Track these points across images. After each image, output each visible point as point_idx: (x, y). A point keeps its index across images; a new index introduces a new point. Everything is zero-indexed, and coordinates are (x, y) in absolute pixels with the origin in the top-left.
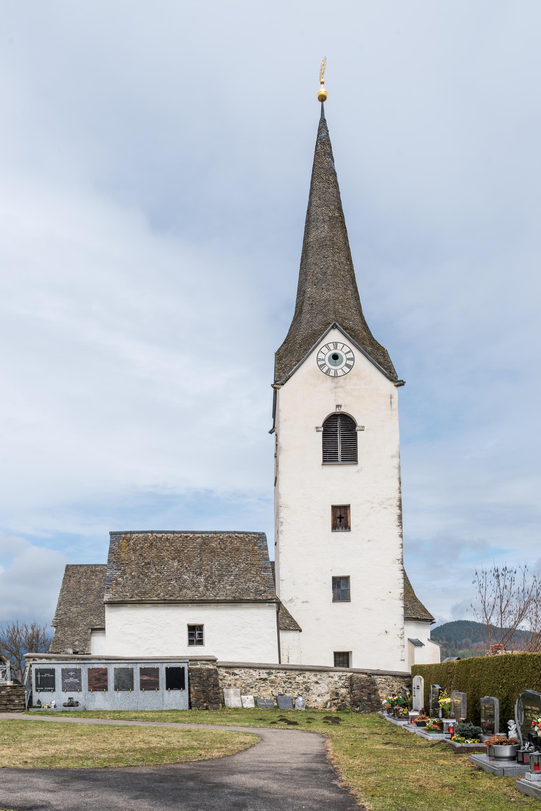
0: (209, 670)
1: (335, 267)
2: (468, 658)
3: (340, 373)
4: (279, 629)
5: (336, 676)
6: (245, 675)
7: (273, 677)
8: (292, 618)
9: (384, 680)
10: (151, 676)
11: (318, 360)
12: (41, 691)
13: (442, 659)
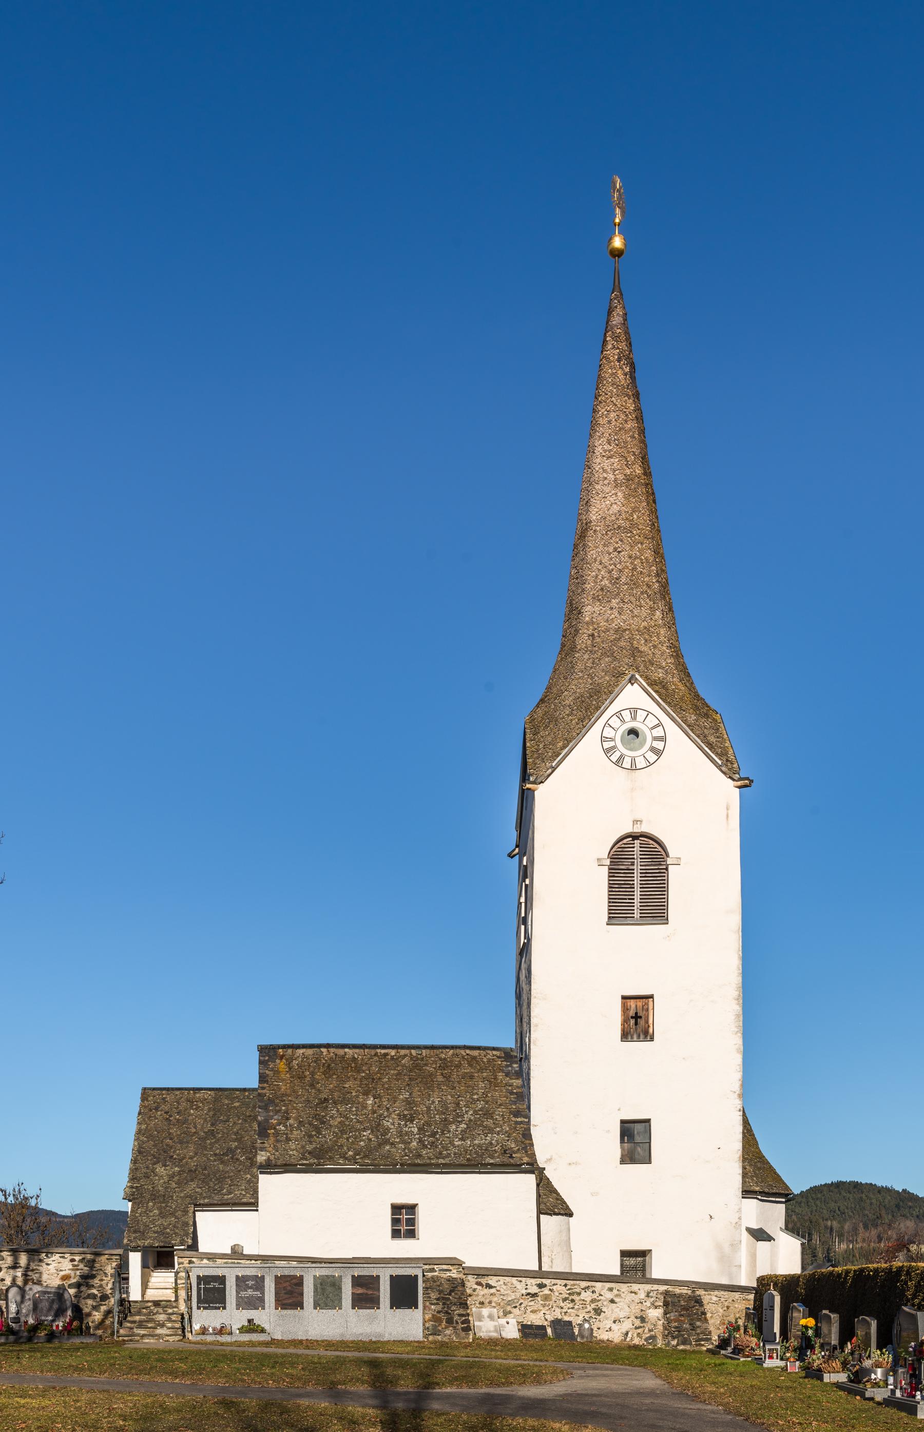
0: (451, 1280)
1: (634, 569)
2: (875, 1265)
3: (640, 763)
4: (540, 1212)
5: (642, 1291)
6: (505, 1287)
7: (546, 1291)
8: (558, 1194)
9: (715, 1299)
10: (367, 1289)
11: (603, 739)
12: (205, 1308)
13: (803, 1268)
